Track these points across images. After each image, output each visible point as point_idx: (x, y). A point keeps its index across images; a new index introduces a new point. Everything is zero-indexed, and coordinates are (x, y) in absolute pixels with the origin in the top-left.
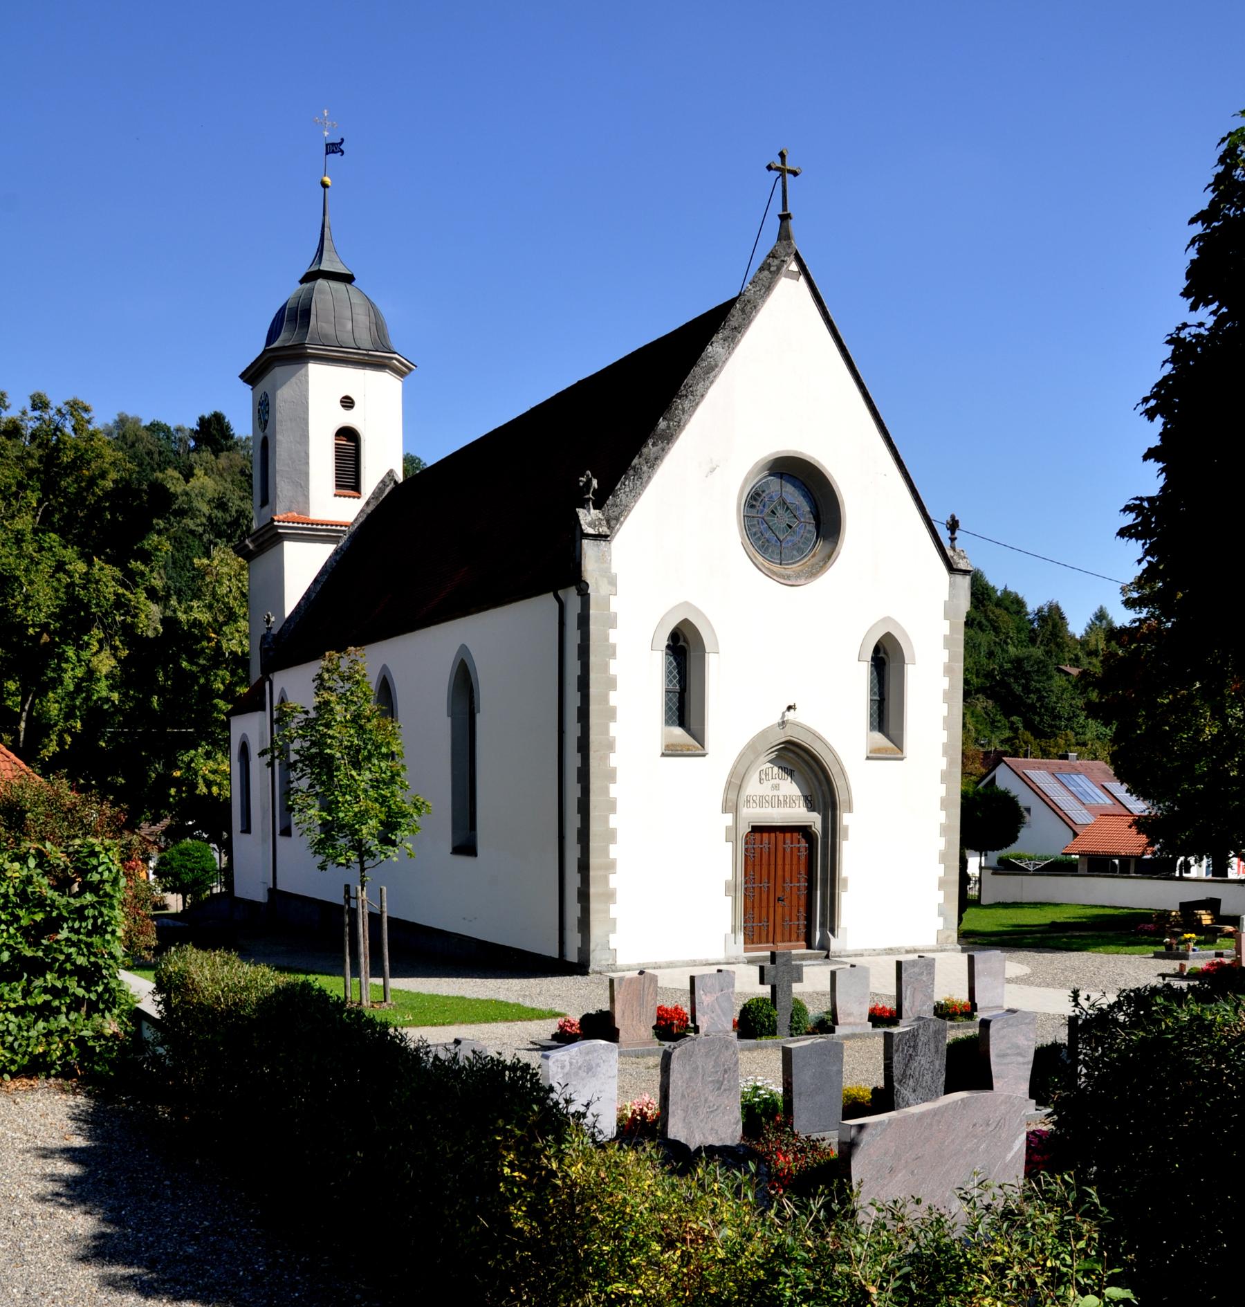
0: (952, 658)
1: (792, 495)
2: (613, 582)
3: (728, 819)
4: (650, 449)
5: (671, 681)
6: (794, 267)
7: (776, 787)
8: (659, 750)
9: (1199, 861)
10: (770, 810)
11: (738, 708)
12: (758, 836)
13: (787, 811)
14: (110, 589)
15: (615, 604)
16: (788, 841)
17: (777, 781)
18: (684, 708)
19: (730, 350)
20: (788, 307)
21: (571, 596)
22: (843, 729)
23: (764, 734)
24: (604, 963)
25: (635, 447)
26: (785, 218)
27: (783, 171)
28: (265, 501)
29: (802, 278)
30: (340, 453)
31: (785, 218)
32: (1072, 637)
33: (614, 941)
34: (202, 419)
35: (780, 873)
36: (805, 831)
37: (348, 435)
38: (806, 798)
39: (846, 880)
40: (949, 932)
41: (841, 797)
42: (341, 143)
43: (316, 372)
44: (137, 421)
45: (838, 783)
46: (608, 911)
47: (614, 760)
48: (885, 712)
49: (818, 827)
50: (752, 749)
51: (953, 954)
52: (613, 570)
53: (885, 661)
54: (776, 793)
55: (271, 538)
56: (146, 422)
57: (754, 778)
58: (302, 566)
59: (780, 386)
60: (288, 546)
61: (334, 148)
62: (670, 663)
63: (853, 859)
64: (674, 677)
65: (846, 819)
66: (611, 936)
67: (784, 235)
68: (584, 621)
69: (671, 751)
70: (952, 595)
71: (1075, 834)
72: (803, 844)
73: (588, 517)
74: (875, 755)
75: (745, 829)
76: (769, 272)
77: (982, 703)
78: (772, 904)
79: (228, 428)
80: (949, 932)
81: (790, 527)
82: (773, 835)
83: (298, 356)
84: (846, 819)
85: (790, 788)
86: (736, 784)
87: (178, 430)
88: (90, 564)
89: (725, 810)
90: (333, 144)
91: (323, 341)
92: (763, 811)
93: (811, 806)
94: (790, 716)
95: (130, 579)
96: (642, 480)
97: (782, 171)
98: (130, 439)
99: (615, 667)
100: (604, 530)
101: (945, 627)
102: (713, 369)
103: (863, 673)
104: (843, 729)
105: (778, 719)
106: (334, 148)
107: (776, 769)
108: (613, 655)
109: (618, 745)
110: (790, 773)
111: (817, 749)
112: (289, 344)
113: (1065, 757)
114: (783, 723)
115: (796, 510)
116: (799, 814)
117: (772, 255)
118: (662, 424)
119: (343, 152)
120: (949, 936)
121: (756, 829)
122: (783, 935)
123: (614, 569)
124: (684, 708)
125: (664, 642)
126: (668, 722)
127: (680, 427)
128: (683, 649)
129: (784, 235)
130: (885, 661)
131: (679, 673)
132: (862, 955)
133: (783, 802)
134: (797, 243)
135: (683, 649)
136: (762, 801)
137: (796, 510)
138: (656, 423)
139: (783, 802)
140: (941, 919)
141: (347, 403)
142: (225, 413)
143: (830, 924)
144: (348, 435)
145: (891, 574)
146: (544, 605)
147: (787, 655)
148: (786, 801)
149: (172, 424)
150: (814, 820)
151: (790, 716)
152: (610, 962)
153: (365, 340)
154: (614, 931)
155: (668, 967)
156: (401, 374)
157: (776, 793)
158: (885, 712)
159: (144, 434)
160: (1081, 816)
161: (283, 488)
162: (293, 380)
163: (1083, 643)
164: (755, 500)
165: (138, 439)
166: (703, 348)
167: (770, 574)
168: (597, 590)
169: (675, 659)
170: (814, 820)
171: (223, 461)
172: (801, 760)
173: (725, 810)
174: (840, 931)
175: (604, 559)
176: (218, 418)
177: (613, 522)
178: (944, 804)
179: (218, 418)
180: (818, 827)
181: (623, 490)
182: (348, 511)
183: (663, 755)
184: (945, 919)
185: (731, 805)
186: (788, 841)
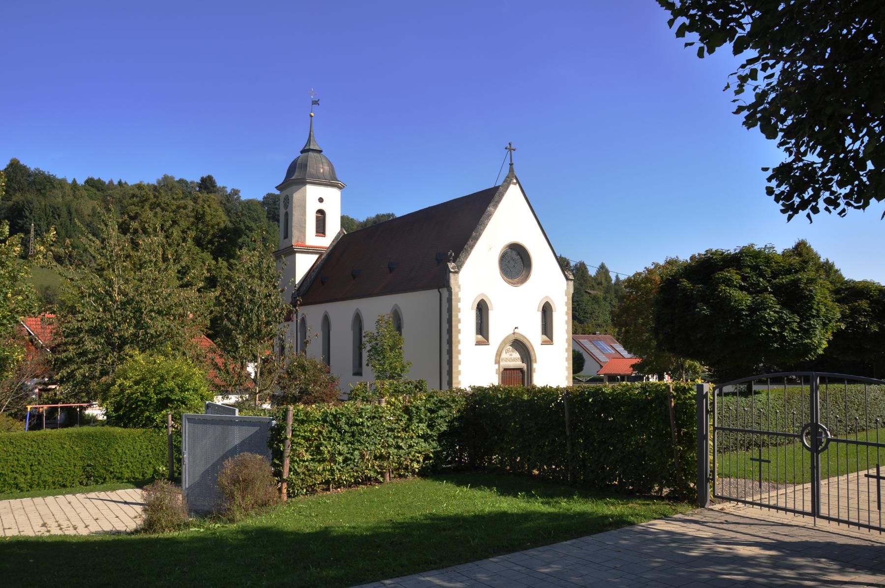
0: (568, 309)
2: (459, 287)
3: (497, 366)
4: (470, 242)
6: (515, 181)
8: (474, 343)
9: (653, 377)
11: (500, 328)
14: (225, 272)
15: (460, 295)
18: (482, 328)
19: (495, 209)
20: (513, 194)
21: (444, 291)
22: (533, 334)
23: (507, 337)
25: (465, 242)
26: (511, 164)
27: (510, 149)
28: (286, 237)
30: (317, 218)
31: (511, 164)
32: (590, 276)
34: (202, 178)
36: (521, 370)
37: (321, 212)
41: (533, 358)
43: (309, 188)
44: (172, 178)
45: (532, 353)
47: (460, 347)
48: (547, 329)
49: (525, 368)
50: (504, 343)
53: (547, 311)
55: (291, 252)
56: (177, 179)
57: (504, 352)
58: (304, 264)
59: (511, 220)
60: (298, 256)
61: (315, 103)
65: (535, 366)
67: (511, 170)
68: (450, 300)
69: (478, 343)
70: (568, 288)
71: (601, 367)
72: (521, 374)
73: (451, 265)
74: (544, 343)
75: (502, 370)
76: (507, 183)
77: (576, 322)
83: (303, 182)
84: (535, 366)
85: (516, 355)
86: (499, 354)
87: (192, 183)
88: (217, 261)
91: (312, 176)
94: (516, 331)
95: (230, 267)
96: (468, 253)
97: (510, 150)
98: (170, 186)
99: (460, 316)
101: (565, 299)
102: (490, 215)
103: (539, 315)
104: (533, 334)
106: (315, 103)
109: (461, 342)
111: (525, 341)
112: (297, 176)
113: (595, 334)
115: (516, 263)
117: (508, 177)
118: (474, 234)
121: (505, 369)
123: (460, 282)
124: (482, 328)
125: (476, 306)
126: (477, 334)
127: (480, 235)
128: (482, 309)
129: (511, 170)
130: (547, 311)
133: (513, 359)
134: (516, 173)
135: (482, 309)
136: (507, 360)
137: (516, 263)
138: (471, 234)
139: (513, 359)
141: (321, 200)
144: (321, 212)
145: (550, 284)
146: (433, 294)
148: (514, 360)
149: (189, 180)
150: (524, 366)
151: (516, 331)
153: (328, 176)
156: (340, 188)
158: (547, 329)
159: (176, 184)
160: (602, 358)
161: (295, 233)
162: (300, 191)
163: (595, 279)
165: (173, 187)
166: (486, 208)
167: (509, 283)
170: (524, 366)
172: (520, 346)
175: (456, 280)
176: (210, 178)
177: (459, 267)
178: (567, 360)
179: (210, 178)
180: (525, 368)
181: (462, 255)
182: (326, 242)
185: (497, 362)
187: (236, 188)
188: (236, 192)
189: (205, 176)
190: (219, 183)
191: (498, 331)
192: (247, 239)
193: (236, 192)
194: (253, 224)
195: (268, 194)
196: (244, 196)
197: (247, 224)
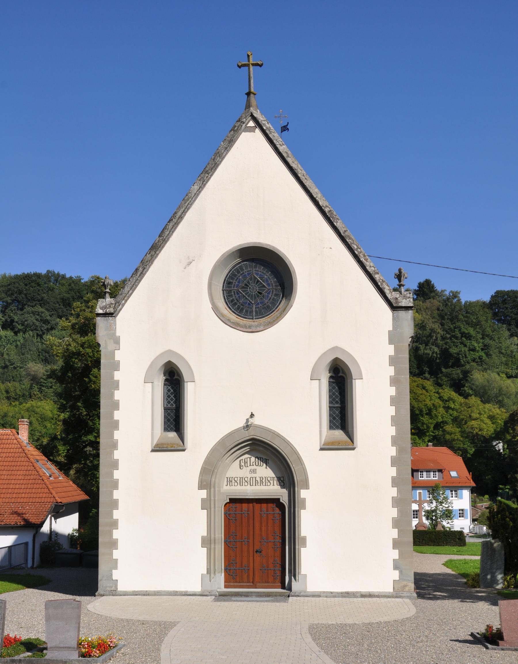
1: (260, 272)
2: (117, 341)
5: (169, 402)
6: (251, 124)
7: (254, 471)
10: (239, 487)
12: (233, 505)
13: (263, 488)
15: (118, 356)
16: (264, 509)
17: (254, 467)
22: (301, 426)
24: (108, 589)
29: (258, 130)
33: (116, 575)
34: (420, 284)
35: (257, 532)
36: (276, 502)
38: (279, 479)
39: (304, 539)
40: (405, 583)
42: (287, 125)
46: (112, 554)
48: (341, 414)
51: (407, 600)
52: (118, 334)
53: (340, 378)
54: (253, 475)
62: (169, 391)
63: (309, 523)
64: (172, 399)
66: (114, 571)
72: (277, 511)
74: (327, 447)
78: (251, 554)
79: (433, 286)
80: (405, 583)
81: (261, 293)
82: (251, 505)
85: (265, 472)
89: (201, 487)
90: (284, 126)
92: (243, 488)
93: (283, 486)
94: (256, 421)
100: (112, 310)
104: (301, 426)
105: (242, 424)
107: (253, 459)
108: (117, 387)
110: (266, 462)
114: (247, 427)
116: (273, 489)
119: (288, 129)
120: (405, 586)
121: (233, 501)
122: (248, 576)
128: (173, 379)
130: (340, 378)
131: (175, 396)
132: (319, 596)
133: (258, 480)
137: (257, 283)
140: (397, 572)
142: (431, 279)
143: (294, 573)
147: (257, 379)
148: (262, 481)
150: (283, 494)
152: (113, 588)
154: (116, 568)
155: (124, 595)
157: (253, 475)
158: (341, 414)
164: (232, 279)
168: (106, 347)
169: (172, 388)
170: (283, 494)
171: (428, 303)
173: (201, 487)
174: (299, 577)
175: (112, 329)
180: (285, 500)
183: (321, 449)
184: (401, 573)
186: (264, 509)
187: (454, 290)
188: (455, 295)
189: (422, 280)
190: (439, 287)
191: (209, 421)
192: (463, 349)
193: (455, 295)
194: (471, 331)
195: (498, 292)
196: (464, 298)
197: (463, 330)
